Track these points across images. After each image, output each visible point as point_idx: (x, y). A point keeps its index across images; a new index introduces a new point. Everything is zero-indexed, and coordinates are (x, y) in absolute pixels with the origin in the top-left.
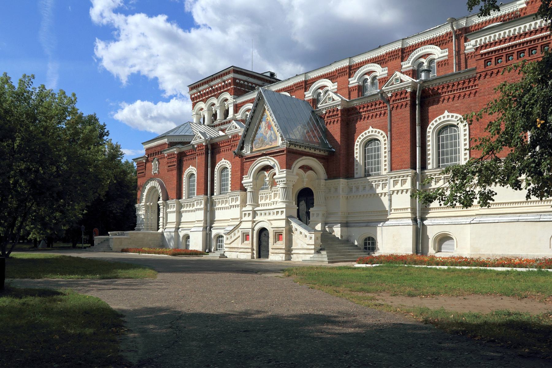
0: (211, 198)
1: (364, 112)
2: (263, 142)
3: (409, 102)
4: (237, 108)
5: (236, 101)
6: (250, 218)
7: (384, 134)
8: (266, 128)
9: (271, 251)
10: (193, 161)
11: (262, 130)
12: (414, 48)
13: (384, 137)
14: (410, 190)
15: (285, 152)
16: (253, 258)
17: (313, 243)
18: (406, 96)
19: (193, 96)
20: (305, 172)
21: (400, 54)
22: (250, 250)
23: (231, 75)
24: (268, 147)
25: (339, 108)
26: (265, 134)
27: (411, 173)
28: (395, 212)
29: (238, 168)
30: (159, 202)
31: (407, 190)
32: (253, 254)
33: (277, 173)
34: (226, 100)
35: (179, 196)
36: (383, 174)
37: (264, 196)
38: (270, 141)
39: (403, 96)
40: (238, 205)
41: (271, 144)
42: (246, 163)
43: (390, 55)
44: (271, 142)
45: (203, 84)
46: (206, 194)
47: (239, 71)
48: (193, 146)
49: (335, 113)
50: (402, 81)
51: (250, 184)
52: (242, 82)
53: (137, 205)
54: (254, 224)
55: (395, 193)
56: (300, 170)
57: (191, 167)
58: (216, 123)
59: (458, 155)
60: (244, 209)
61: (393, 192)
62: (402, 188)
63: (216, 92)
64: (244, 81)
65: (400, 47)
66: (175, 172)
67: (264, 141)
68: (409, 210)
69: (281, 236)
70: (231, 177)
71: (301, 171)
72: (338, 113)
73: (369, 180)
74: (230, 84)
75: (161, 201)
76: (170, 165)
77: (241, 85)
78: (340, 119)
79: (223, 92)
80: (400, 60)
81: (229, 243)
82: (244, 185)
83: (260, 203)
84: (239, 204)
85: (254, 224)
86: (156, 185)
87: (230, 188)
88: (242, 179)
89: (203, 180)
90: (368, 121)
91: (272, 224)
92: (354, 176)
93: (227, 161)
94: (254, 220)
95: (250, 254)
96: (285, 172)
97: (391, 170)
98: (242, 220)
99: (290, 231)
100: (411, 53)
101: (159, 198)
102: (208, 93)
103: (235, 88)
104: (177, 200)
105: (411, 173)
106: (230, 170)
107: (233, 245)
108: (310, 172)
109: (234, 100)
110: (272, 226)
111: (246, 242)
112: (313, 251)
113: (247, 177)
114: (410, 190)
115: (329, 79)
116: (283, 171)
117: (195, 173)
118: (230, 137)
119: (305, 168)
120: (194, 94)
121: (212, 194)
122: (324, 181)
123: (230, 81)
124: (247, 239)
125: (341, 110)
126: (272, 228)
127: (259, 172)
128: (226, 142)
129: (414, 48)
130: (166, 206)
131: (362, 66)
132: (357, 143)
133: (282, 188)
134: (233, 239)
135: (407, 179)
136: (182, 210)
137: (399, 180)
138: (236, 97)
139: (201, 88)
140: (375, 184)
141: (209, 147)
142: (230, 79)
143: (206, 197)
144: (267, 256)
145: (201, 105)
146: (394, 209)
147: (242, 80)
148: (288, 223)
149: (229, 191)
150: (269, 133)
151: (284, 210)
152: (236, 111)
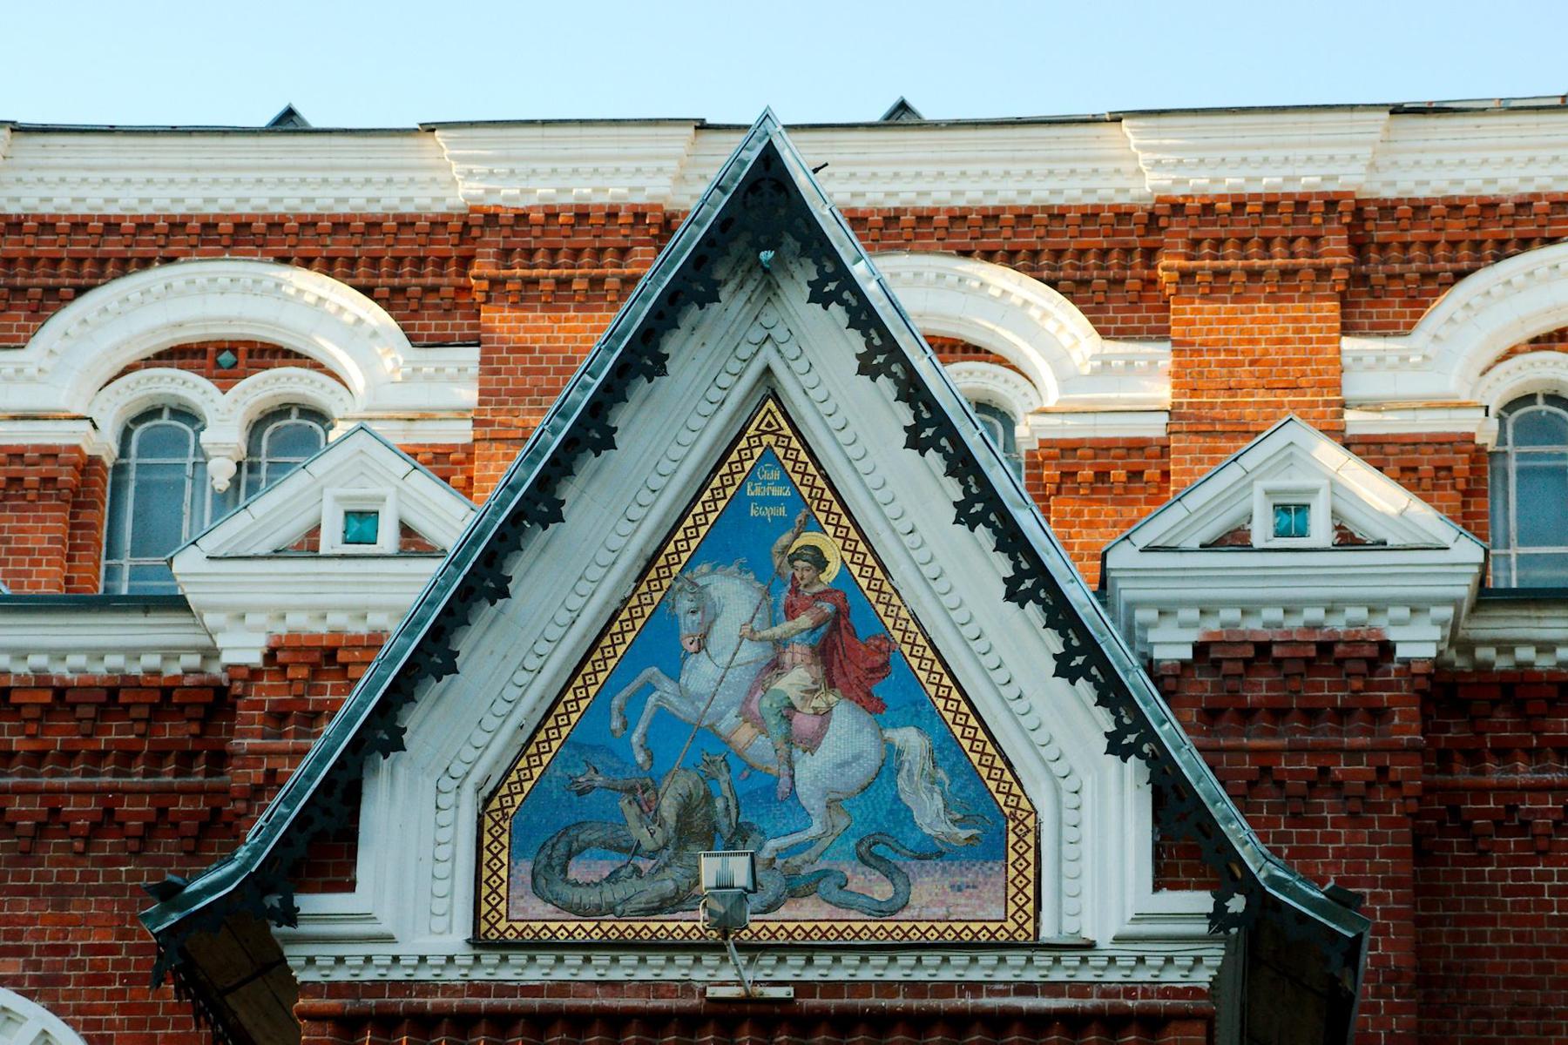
8: (775, 666)
11: (701, 673)
26: (759, 747)
38: (868, 858)
44: (891, 872)
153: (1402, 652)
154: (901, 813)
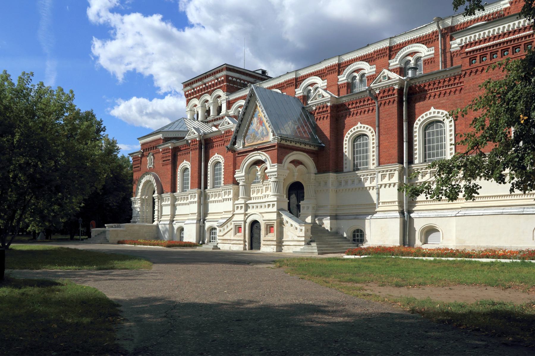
0: (205, 192)
1: (352, 108)
2: (255, 137)
3: (396, 99)
4: (230, 104)
5: (229, 98)
6: (242, 211)
7: (372, 130)
9: (262, 242)
10: (187, 156)
11: (254, 125)
12: (401, 46)
15: (276, 147)
16: (245, 249)
17: (304, 235)
19: (187, 93)
20: (296, 166)
21: (388, 52)
22: (242, 242)
23: (224, 73)
24: (259, 142)
25: (329, 104)
26: (257, 130)
28: (383, 205)
29: (231, 163)
30: (154, 196)
31: (395, 184)
32: (245, 245)
33: (269, 167)
34: (219, 97)
35: (174, 190)
36: (371, 168)
38: (262, 137)
39: (390, 93)
41: (262, 139)
42: (238, 158)
43: (378, 53)
44: (263, 137)
45: (196, 81)
46: (200, 188)
47: (231, 69)
48: (187, 141)
49: (325, 109)
50: (389, 79)
51: (242, 178)
52: (234, 79)
53: (132, 199)
54: (247, 216)
56: (291, 164)
57: (185, 161)
58: (209, 119)
60: (236, 202)
61: (381, 185)
63: (209, 89)
64: (237, 78)
65: (388, 45)
66: (169, 167)
67: (256, 136)
68: (397, 203)
69: (272, 228)
70: (224, 172)
71: (292, 166)
72: (327, 109)
74: (223, 81)
75: (156, 195)
76: (165, 159)
77: (234, 83)
78: (329, 115)
79: (216, 89)
80: (388, 58)
81: (222, 235)
82: (236, 179)
83: (252, 196)
84: (232, 197)
85: (247, 216)
87: (222, 182)
88: (234, 173)
89: (196, 175)
90: (357, 117)
91: (263, 217)
93: (220, 156)
94: (246, 212)
95: (242, 246)
96: (276, 166)
97: (379, 164)
98: (234, 213)
99: (281, 223)
100: (398, 52)
101: (154, 192)
102: (201, 90)
103: (227, 85)
104: (172, 194)
106: (223, 165)
107: (226, 237)
108: (300, 166)
109: (227, 97)
110: (264, 219)
111: (238, 234)
112: (303, 243)
113: (239, 171)
115: (319, 77)
116: (274, 166)
117: (189, 167)
118: (223, 132)
119: (296, 163)
120: (188, 91)
121: (206, 187)
122: (314, 175)
123: (223, 78)
124: (239, 231)
125: (331, 106)
126: (264, 220)
127: (251, 166)
128: (219, 137)
129: (401, 46)
130: (161, 199)
131: (351, 64)
133: (273, 181)
134: (226, 231)
135: (394, 173)
136: (177, 203)
138: (228, 93)
139: (194, 85)
140: (364, 178)
141: (203, 142)
142: (223, 76)
143: (200, 190)
144: (259, 248)
145: (195, 101)
146: (382, 203)
147: (234, 77)
148: (279, 215)
149: (222, 185)
150: (261, 128)
151: (275, 203)
152: (229, 107)
154: (263, 133)
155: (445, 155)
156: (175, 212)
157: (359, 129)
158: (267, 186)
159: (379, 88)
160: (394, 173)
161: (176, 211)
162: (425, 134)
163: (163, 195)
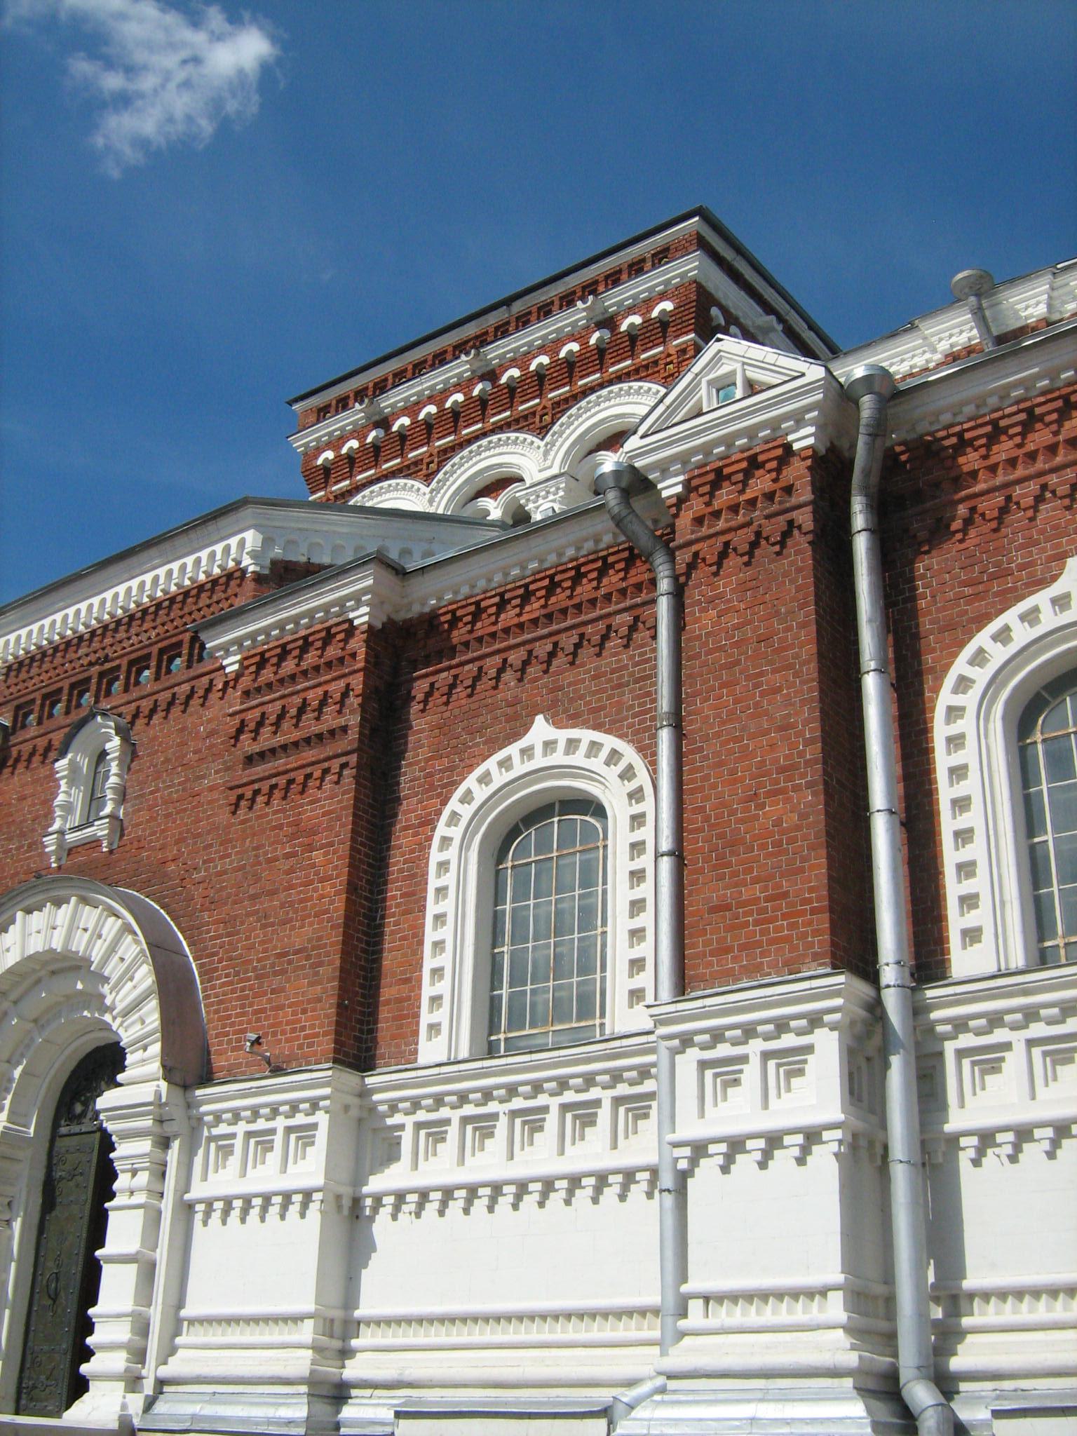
0: (917, 1010)
3: (805, 518)
7: (630, 754)
13: (628, 774)
14: (838, 1134)
18: (782, 483)
27: (838, 1002)
28: (712, 1322)
31: (812, 1136)
36: (620, 1029)
37: (606, 1096)
39: (332, 652)
40: (307, 1195)
49: (332, 652)
50: (752, 388)
55: (708, 1167)
59: (598, 976)
61: (699, 1149)
62: (518, 1170)
68: (835, 1309)
73: (376, 1097)
78: (357, 682)
86: (113, 970)
92: (416, 1052)
97: (682, 986)
104: (350, 1078)
105: (838, 1002)
114: (838, 1134)
125: (371, 629)
132: (971, 672)
135: (809, 1049)
136: (376, 1183)
137: (744, 1059)
146: (707, 1299)
153: (796, 446)
155: (603, 1015)
156: (350, 1296)
157: (539, 761)
158: (261, 1124)
159: (683, 458)
160: (809, 1049)
161: (369, 1278)
162: (498, 876)
163: (213, 1100)
